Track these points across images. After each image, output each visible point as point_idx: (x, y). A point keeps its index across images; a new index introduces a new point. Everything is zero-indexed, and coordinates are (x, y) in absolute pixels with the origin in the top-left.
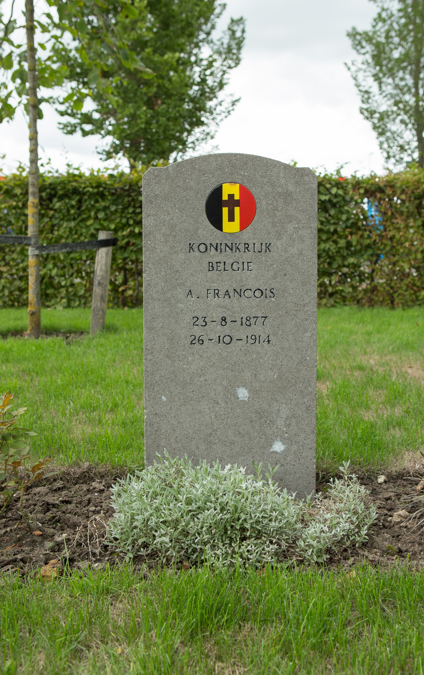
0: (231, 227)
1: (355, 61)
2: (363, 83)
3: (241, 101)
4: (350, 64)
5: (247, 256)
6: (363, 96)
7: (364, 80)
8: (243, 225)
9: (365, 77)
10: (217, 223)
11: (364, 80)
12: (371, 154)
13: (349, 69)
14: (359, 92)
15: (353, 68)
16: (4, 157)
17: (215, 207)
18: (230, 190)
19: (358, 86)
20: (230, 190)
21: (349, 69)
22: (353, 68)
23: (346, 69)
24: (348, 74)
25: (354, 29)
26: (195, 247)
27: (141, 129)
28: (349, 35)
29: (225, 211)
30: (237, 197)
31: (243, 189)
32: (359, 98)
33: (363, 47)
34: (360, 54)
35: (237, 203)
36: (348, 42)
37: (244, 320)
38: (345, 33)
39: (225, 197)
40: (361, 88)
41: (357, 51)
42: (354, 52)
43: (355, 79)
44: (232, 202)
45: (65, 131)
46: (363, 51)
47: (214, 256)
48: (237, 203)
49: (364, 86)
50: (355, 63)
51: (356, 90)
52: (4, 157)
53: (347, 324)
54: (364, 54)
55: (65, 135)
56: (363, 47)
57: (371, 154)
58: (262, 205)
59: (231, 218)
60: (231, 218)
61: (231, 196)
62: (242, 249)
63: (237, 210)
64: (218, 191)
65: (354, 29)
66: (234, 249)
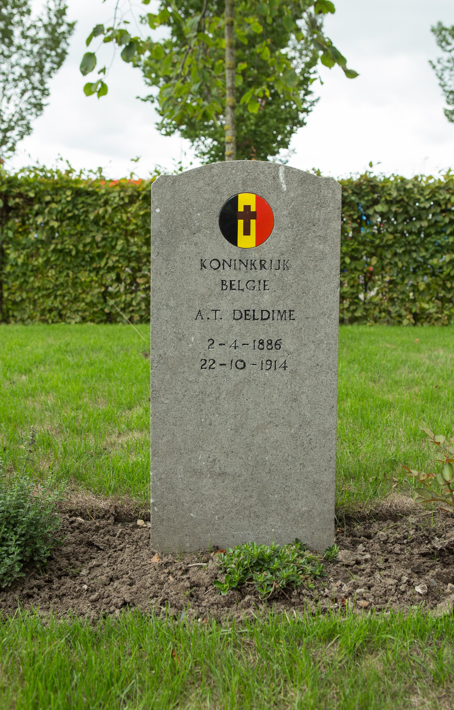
0: (246, 241)
1: (442, 58)
2: (449, 83)
3: (320, 102)
4: (435, 63)
5: (263, 274)
6: (448, 97)
7: (450, 79)
8: (260, 240)
9: (451, 76)
10: (232, 238)
11: (450, 79)
12: (426, 158)
13: (434, 67)
14: (444, 93)
15: (439, 67)
18: (246, 200)
19: (443, 86)
20: (246, 200)
21: (434, 67)
22: (439, 67)
23: (431, 67)
24: (433, 72)
25: (440, 24)
26: (207, 264)
27: (251, 130)
28: (433, 30)
29: (241, 223)
30: (253, 209)
31: (260, 201)
32: (444, 98)
33: (448, 44)
34: (445, 51)
35: (254, 215)
36: (433, 38)
37: (257, 344)
38: (429, 28)
39: (241, 209)
40: (447, 88)
41: (442, 47)
42: (439, 49)
43: (440, 78)
44: (248, 214)
45: (163, 131)
46: (449, 48)
47: (228, 274)
48: (254, 215)
49: (450, 86)
50: (441, 61)
51: (440, 90)
53: (386, 342)
54: (450, 51)
55: (164, 137)
56: (448, 44)
57: (426, 158)
58: (281, 216)
59: (247, 232)
60: (247, 232)
61: (247, 208)
62: (258, 267)
63: (253, 222)
64: (234, 201)
65: (440, 24)
66: (249, 266)
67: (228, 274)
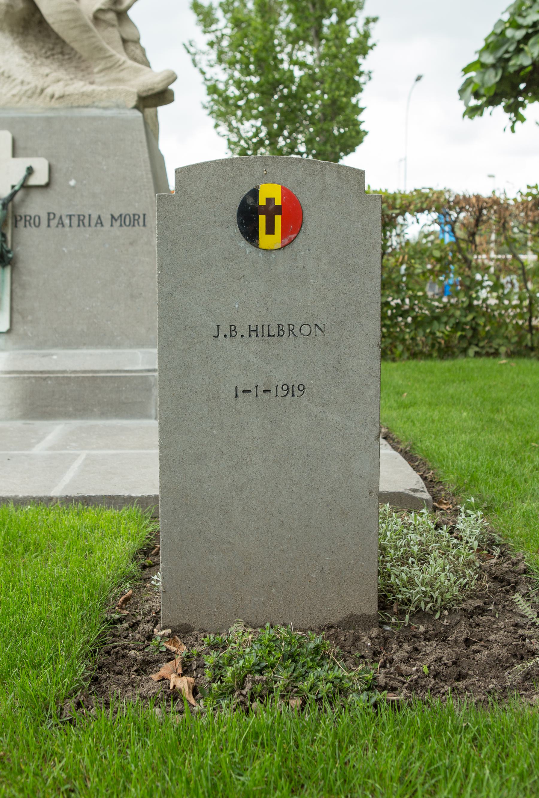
10: (251, 236)
29: (262, 219)
35: (278, 210)
39: (262, 202)
44: (271, 210)
59: (270, 230)
60: (270, 230)
63: (278, 219)
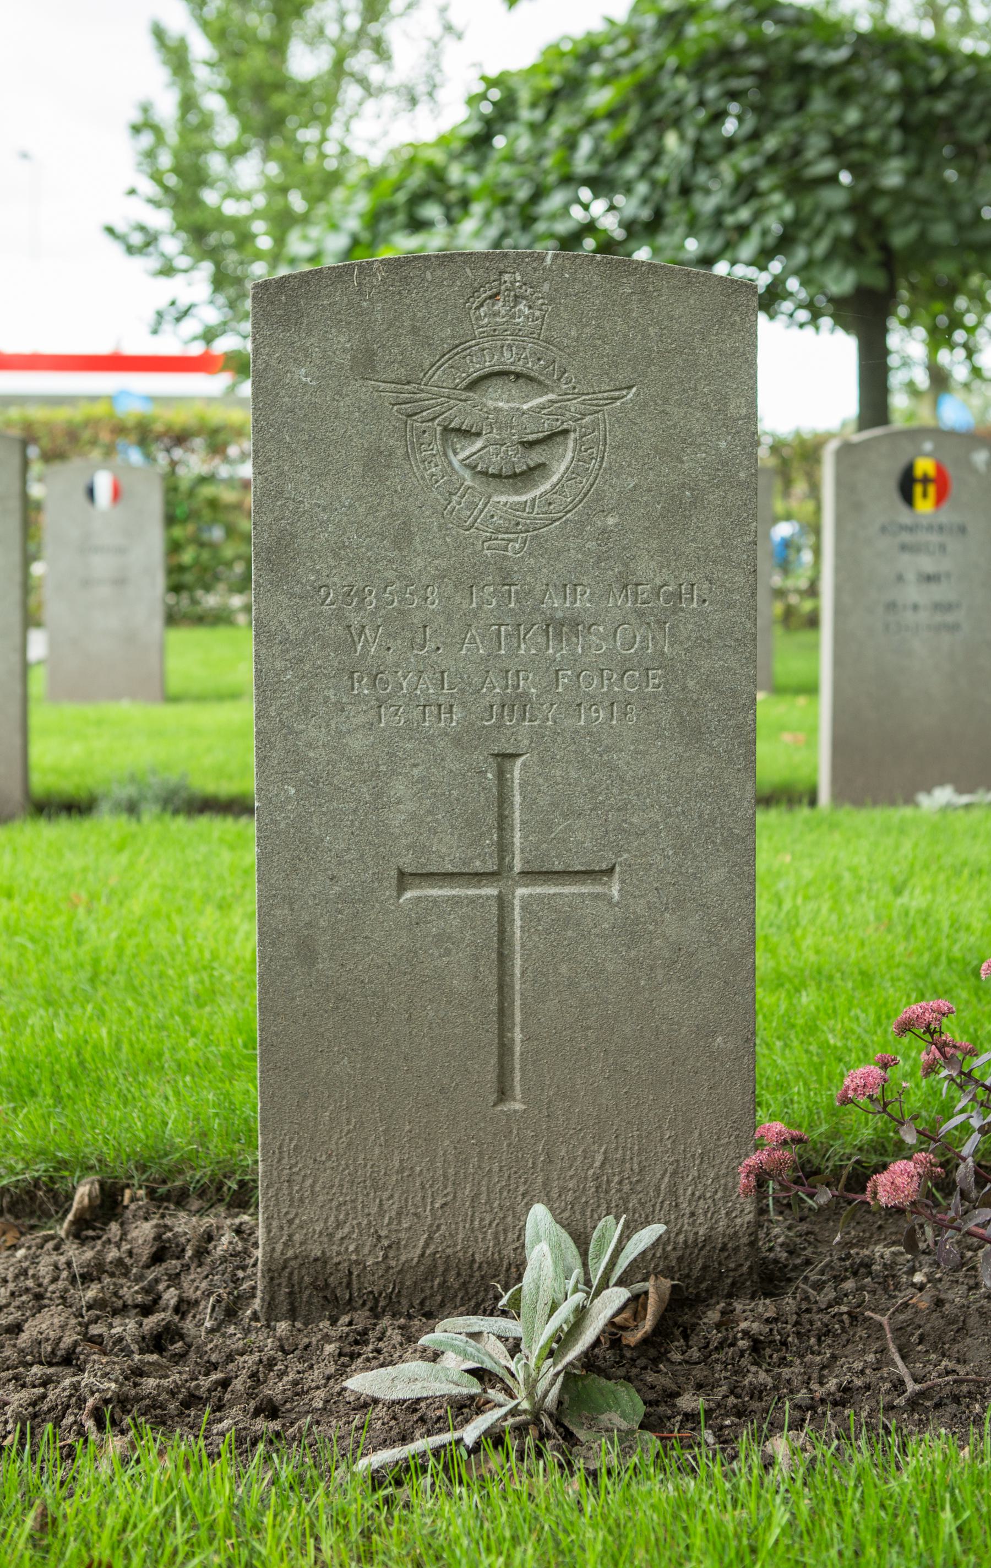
0: (924, 506)
16: (25, 156)
17: (907, 485)
18: (925, 466)
44: (925, 480)
47: (906, 537)
52: (25, 156)
59: (925, 495)
60: (925, 495)
67: (906, 537)
